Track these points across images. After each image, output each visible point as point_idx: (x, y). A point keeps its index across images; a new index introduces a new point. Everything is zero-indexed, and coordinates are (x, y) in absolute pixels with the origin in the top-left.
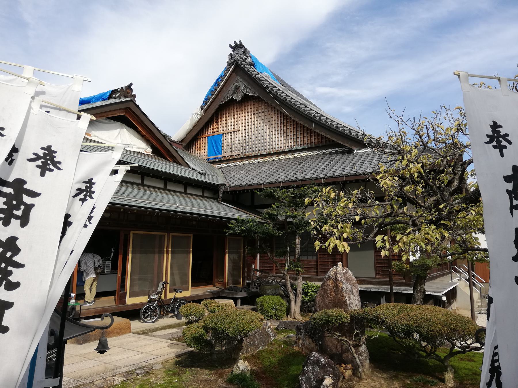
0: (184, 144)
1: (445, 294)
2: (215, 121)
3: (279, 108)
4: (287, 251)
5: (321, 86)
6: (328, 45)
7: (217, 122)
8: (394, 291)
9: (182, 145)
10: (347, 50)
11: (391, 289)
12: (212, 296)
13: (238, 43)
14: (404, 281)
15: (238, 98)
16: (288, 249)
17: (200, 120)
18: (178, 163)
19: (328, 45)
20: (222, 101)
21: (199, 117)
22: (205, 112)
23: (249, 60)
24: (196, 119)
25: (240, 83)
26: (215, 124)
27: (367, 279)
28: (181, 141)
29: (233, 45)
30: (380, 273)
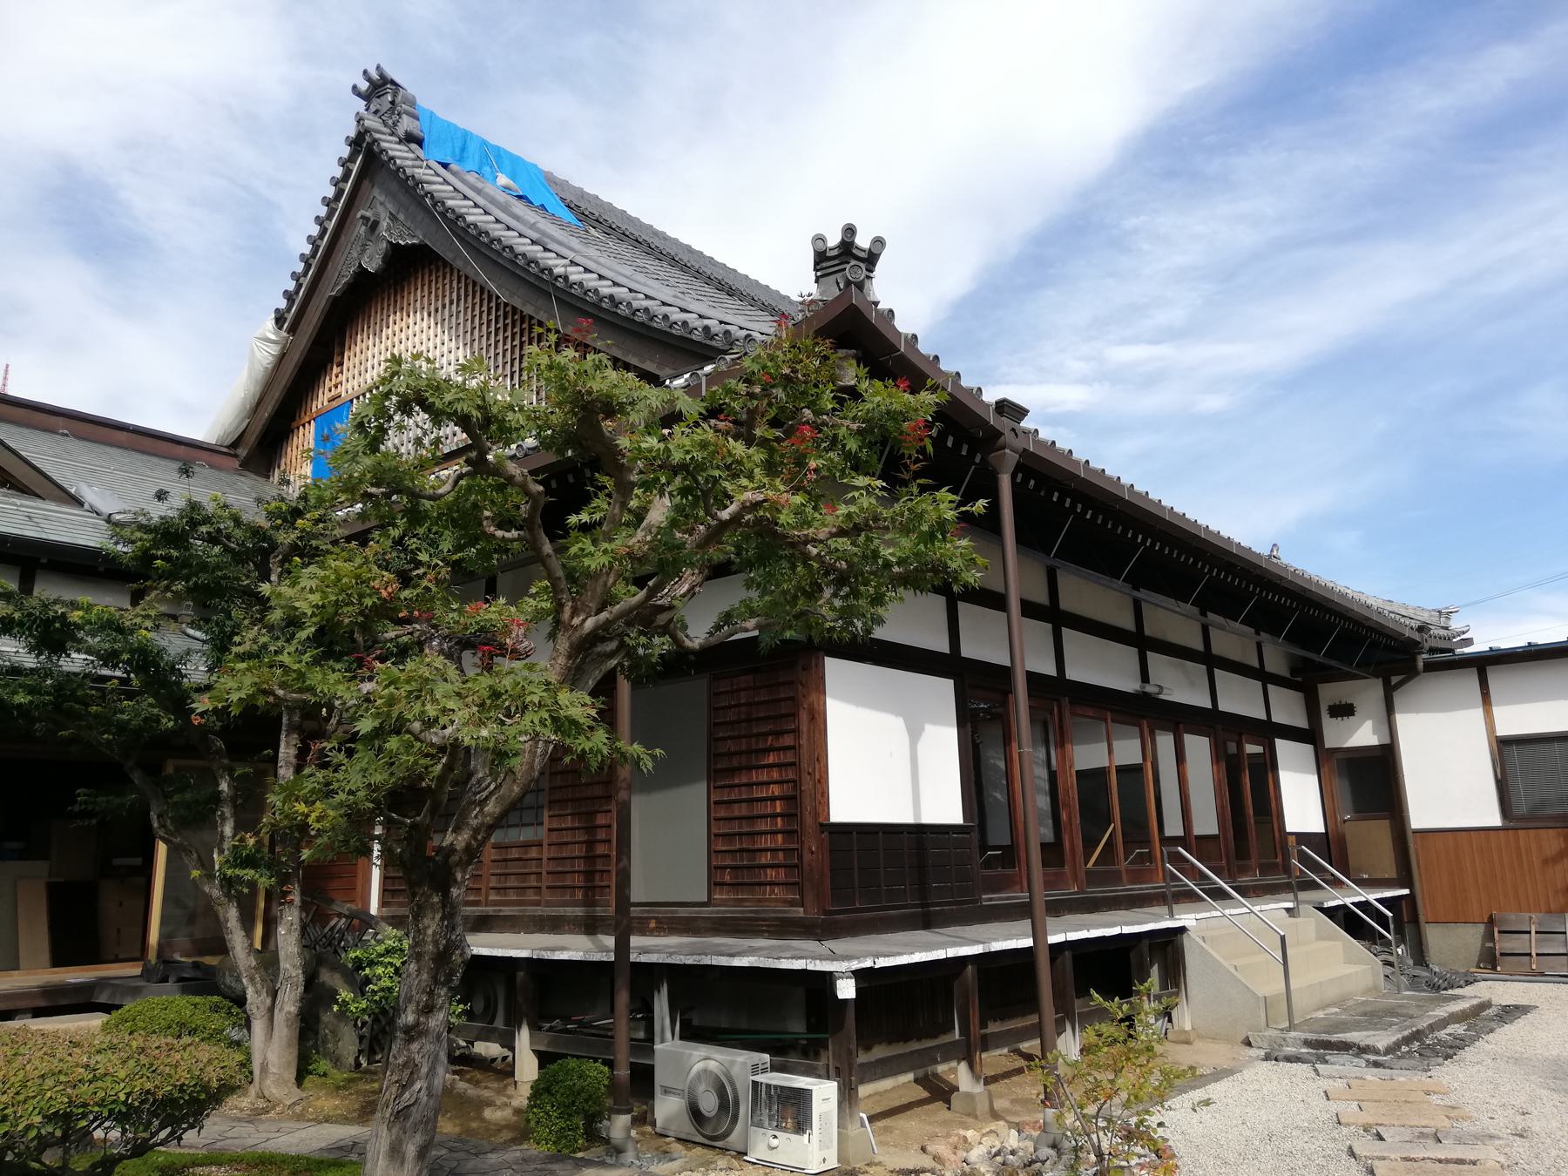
0: (243, 452)
1: (858, 975)
2: (336, 359)
3: (472, 275)
4: (216, 798)
5: (1123, 342)
6: (1132, 222)
7: (341, 364)
8: (633, 958)
9: (236, 456)
10: (1191, 233)
11: (622, 947)
12: (42, 1003)
13: (375, 76)
14: (800, 912)
15: (372, 263)
16: (224, 786)
17: (281, 358)
18: (23, 490)
19: (1132, 222)
20: (335, 284)
21: (275, 350)
22: (292, 330)
23: (406, 124)
24: (265, 355)
25: (380, 209)
26: (335, 370)
27: (683, 912)
28: (235, 444)
29: (364, 86)
30: (727, 878)
